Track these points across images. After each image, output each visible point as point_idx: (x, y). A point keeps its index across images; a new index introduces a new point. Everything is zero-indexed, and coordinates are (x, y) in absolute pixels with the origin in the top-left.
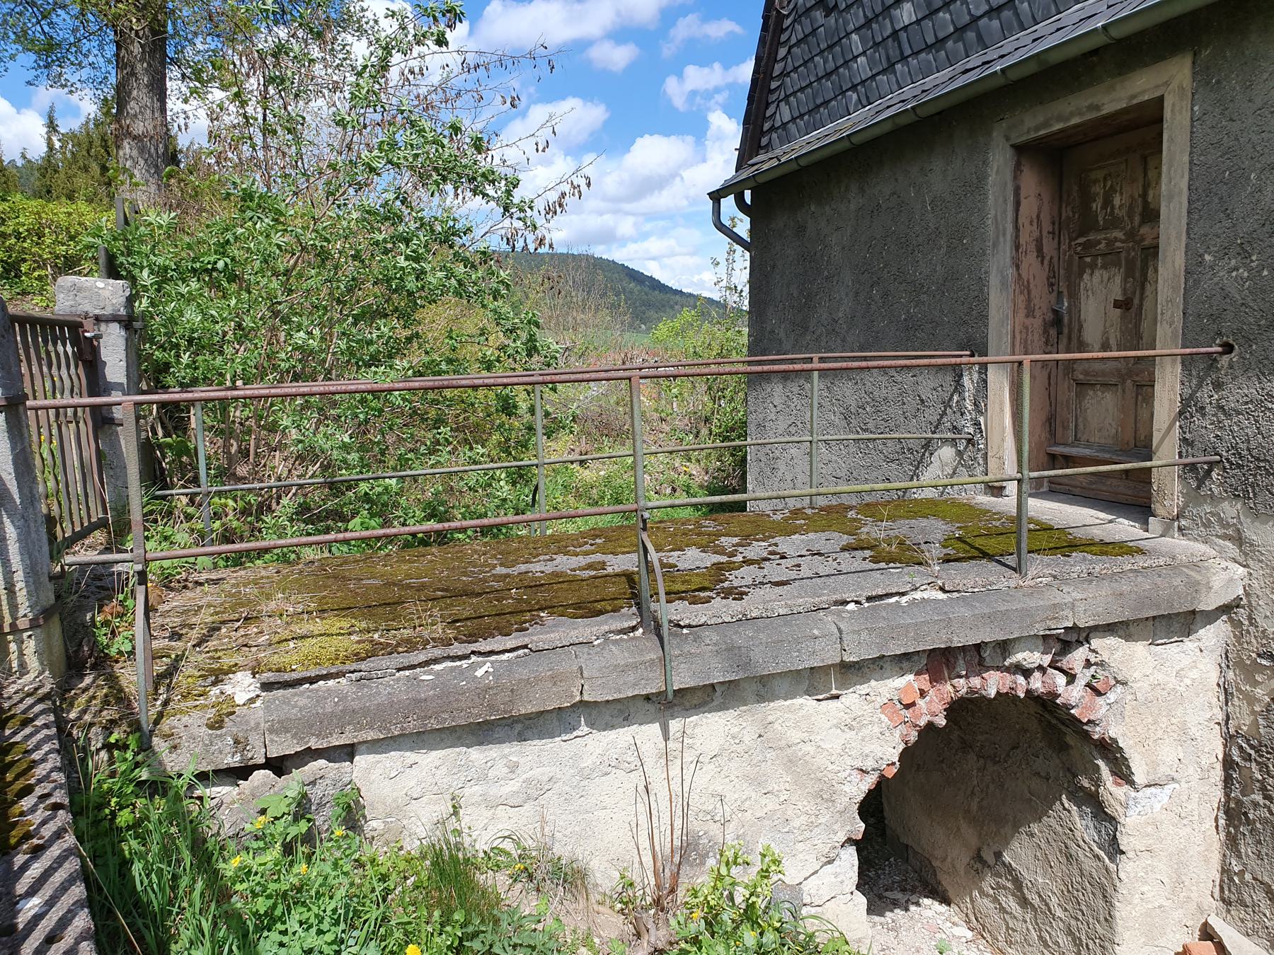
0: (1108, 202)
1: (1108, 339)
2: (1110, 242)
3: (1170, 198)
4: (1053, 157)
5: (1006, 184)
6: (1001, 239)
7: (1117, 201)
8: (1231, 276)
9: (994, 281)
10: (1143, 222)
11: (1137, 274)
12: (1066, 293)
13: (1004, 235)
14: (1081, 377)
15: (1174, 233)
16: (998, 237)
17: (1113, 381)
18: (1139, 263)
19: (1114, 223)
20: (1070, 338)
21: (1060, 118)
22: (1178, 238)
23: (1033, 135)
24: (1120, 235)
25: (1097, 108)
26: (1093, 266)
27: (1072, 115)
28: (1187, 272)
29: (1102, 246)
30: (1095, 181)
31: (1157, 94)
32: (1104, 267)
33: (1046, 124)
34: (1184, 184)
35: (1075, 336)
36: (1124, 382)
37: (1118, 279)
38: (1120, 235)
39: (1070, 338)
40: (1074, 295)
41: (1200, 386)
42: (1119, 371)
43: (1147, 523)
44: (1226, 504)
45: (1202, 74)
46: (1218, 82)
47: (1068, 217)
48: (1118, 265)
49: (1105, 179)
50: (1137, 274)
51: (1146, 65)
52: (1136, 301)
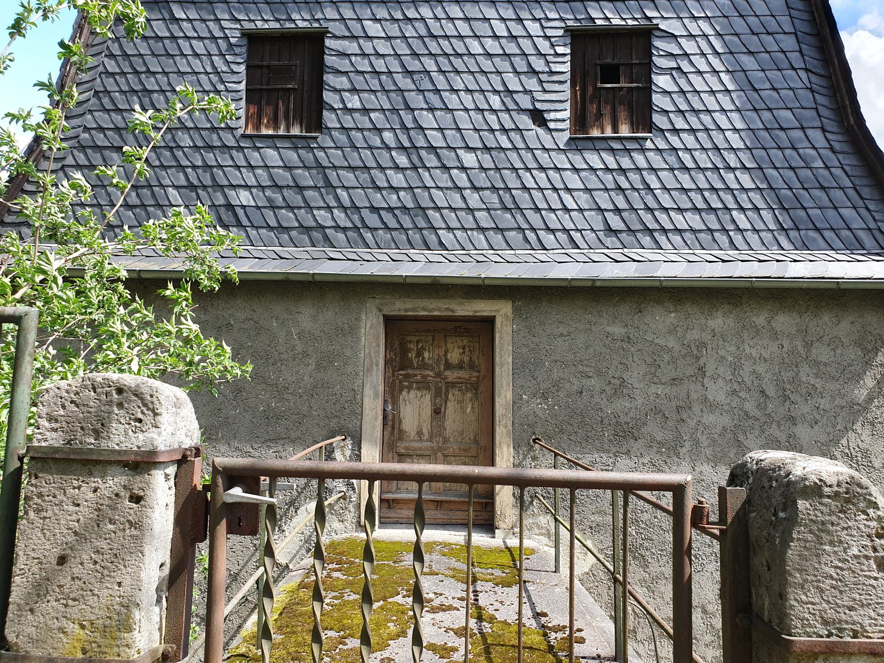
0: (419, 354)
1: (421, 429)
2: (423, 377)
3: (502, 365)
4: (393, 325)
5: (379, 336)
6: (375, 368)
7: (426, 355)
8: (538, 407)
9: (368, 392)
10: (445, 369)
11: (443, 396)
12: (390, 400)
13: (377, 365)
14: (403, 451)
15: (505, 383)
16: (372, 366)
17: (428, 453)
18: (443, 389)
19: (424, 366)
20: (393, 428)
21: (424, 309)
22: (508, 385)
23: (403, 313)
24: (431, 374)
25: (452, 311)
26: (409, 388)
27: (434, 309)
28: (514, 402)
29: (419, 377)
30: (410, 342)
31: (493, 314)
32: (418, 389)
33: (414, 310)
34: (510, 360)
35: (397, 426)
36: (436, 454)
37: (428, 397)
38: (431, 374)
39: (393, 428)
40: (395, 403)
41: (524, 458)
42: (432, 448)
43: (494, 533)
44: (541, 518)
45: (515, 310)
46: (526, 318)
47: (391, 358)
48: (428, 388)
49: (418, 342)
50: (443, 396)
51: (482, 298)
52: (443, 410)
